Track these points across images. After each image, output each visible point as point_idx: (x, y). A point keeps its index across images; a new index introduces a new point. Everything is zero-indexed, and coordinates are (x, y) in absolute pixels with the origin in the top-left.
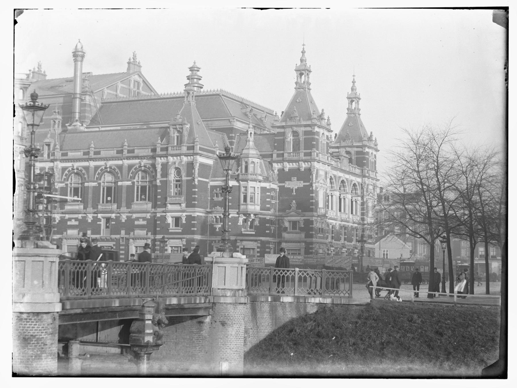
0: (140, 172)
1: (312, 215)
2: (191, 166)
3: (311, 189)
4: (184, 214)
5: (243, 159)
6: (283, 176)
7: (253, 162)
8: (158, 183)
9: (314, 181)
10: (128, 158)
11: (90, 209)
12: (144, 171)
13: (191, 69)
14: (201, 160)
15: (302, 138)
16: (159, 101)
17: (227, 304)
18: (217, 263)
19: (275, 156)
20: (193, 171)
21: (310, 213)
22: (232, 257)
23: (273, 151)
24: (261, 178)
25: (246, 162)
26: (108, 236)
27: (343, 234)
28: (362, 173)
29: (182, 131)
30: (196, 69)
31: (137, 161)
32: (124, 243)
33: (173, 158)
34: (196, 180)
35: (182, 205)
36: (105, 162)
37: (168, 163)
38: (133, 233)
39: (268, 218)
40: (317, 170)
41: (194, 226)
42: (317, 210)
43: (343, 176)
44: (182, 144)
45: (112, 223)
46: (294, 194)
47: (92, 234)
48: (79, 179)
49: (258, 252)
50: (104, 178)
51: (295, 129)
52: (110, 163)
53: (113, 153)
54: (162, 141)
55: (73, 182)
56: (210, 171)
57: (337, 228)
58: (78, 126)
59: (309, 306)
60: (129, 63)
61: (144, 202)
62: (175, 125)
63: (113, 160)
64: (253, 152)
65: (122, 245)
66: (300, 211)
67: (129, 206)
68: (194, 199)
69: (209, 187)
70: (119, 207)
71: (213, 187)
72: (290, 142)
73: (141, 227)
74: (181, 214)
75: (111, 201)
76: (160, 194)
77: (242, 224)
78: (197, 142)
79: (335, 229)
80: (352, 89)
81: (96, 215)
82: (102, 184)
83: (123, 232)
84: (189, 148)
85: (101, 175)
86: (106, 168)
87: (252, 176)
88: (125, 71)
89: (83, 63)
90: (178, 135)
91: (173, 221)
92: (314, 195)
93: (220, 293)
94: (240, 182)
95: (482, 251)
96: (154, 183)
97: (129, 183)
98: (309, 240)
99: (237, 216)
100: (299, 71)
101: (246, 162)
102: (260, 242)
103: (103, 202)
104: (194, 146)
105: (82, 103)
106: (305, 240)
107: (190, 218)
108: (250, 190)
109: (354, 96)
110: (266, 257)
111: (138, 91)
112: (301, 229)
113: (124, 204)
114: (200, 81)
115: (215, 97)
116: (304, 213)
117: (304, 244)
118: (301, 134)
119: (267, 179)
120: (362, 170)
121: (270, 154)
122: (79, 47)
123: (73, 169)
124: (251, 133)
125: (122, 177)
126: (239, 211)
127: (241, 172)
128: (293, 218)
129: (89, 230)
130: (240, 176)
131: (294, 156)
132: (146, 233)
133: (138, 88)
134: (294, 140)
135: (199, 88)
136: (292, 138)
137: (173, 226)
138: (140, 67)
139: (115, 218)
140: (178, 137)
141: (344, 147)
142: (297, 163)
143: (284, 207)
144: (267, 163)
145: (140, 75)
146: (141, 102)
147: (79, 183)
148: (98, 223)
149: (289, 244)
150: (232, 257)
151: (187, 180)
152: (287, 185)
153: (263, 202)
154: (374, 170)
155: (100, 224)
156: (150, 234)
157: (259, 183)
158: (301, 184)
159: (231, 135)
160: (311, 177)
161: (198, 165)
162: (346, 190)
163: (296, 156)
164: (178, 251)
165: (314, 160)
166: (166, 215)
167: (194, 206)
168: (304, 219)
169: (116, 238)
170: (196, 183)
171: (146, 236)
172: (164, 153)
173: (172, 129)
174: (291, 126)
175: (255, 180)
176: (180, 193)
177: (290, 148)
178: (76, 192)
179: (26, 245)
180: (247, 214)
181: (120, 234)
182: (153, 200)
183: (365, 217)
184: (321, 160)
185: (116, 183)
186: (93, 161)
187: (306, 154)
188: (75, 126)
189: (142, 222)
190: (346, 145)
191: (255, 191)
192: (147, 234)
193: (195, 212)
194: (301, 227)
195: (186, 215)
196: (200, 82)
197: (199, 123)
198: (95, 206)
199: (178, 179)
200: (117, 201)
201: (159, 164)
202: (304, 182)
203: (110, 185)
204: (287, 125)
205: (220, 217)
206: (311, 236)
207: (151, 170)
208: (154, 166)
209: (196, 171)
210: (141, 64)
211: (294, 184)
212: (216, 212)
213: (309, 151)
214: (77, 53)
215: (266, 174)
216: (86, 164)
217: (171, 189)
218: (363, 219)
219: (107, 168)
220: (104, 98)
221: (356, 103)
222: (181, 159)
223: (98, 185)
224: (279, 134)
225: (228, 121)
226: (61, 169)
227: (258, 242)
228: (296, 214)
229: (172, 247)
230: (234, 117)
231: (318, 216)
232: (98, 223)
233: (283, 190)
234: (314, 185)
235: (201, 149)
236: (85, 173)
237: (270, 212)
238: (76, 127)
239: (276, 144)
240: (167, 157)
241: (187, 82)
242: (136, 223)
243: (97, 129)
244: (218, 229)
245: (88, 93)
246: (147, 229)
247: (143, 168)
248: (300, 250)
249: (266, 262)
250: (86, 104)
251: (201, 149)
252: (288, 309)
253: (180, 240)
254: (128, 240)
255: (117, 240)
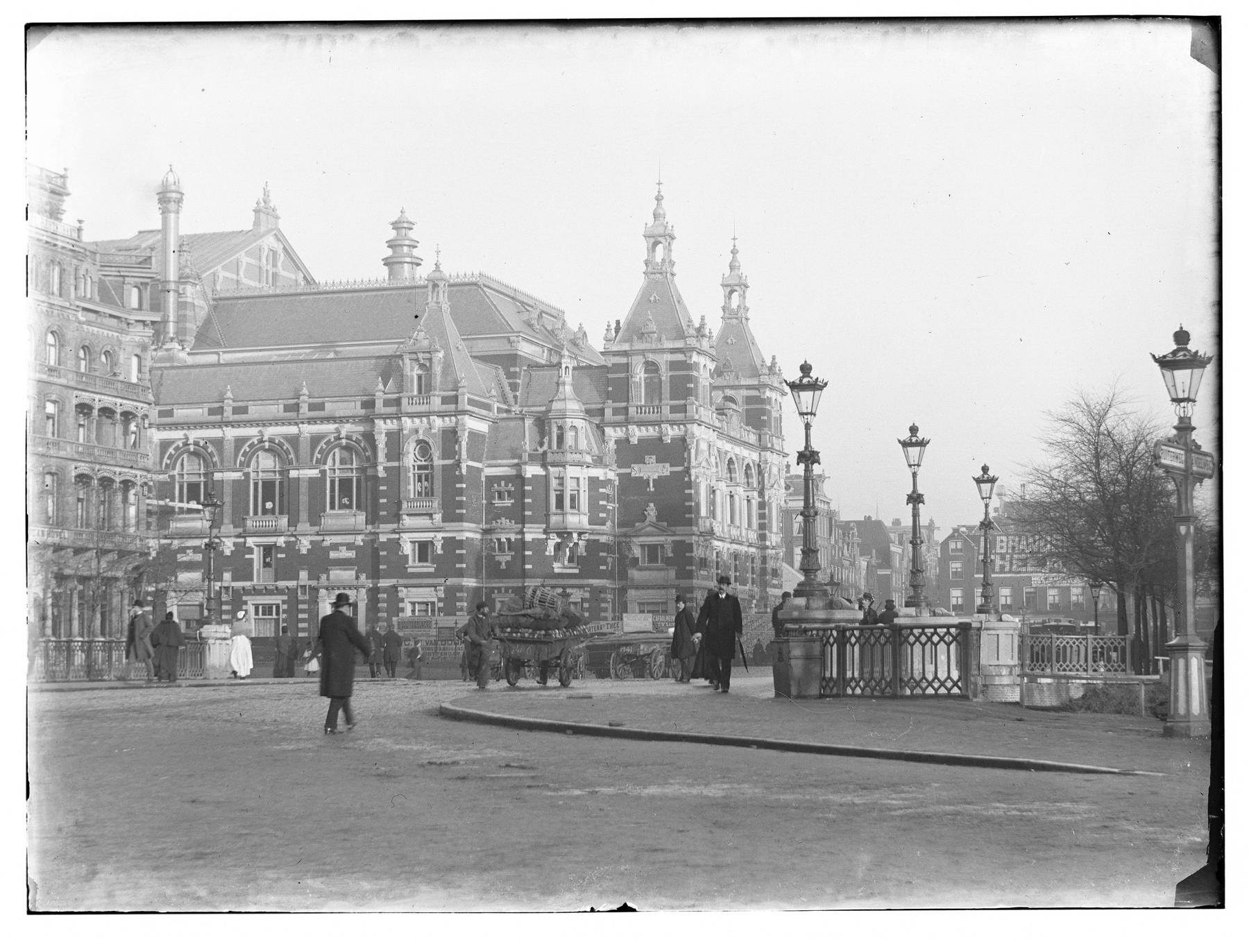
0: (337, 450)
1: (691, 532)
2: (451, 436)
3: (686, 479)
4: (440, 535)
5: (552, 421)
6: (628, 453)
7: (574, 428)
8: (381, 473)
9: (693, 463)
10: (312, 421)
11: (227, 528)
12: (347, 448)
13: (396, 226)
14: (471, 424)
15: (665, 375)
16: (344, 295)
17: (1003, 686)
18: (987, 629)
19: (608, 412)
20: (457, 446)
21: (686, 529)
22: (1001, 620)
23: (604, 403)
24: (588, 459)
25: (560, 428)
26: (271, 584)
27: (733, 569)
28: (760, 441)
29: (431, 365)
30: (406, 225)
31: (330, 427)
32: (307, 597)
33: (413, 422)
34: (464, 466)
35: (434, 516)
36: (259, 428)
37: (400, 430)
38: (325, 575)
39: (603, 539)
40: (697, 441)
41: (461, 559)
42: (697, 520)
43: (729, 449)
44: (432, 393)
45: (279, 556)
46: (652, 489)
47: (234, 579)
48: (200, 464)
49: (605, 610)
50: (257, 462)
51: (651, 357)
52: (270, 431)
53: (276, 410)
54: (385, 387)
55: (185, 471)
56: (484, 445)
57: (725, 558)
58: (176, 351)
59: (1072, 688)
60: (257, 211)
61: (348, 511)
62: (415, 353)
63: (277, 424)
64: (573, 406)
65: (303, 602)
66: (665, 524)
67: (315, 519)
68: (460, 505)
69: (483, 479)
70: (293, 522)
71: (491, 480)
72: (641, 384)
73: (343, 563)
74: (432, 535)
75: (273, 511)
76: (531, 507)
77: (553, 554)
78: (463, 387)
79: (722, 559)
80: (730, 266)
81: (242, 540)
82: (253, 475)
83: (303, 575)
84: (445, 400)
85: (249, 457)
86: (261, 441)
87: (574, 455)
88: (248, 226)
89: (181, 215)
90: (420, 372)
91: (414, 550)
92: (693, 491)
93: (993, 671)
94: (549, 467)
95: (1006, 596)
96: (370, 472)
97: (314, 473)
98: (684, 583)
99: (544, 536)
100: (654, 237)
101: (560, 428)
102: (589, 589)
103: (256, 513)
104: (456, 397)
105: (180, 299)
106: (677, 582)
107: (450, 544)
108: (570, 486)
109: (737, 282)
110: (625, 619)
111: (274, 270)
112: (668, 562)
113: (304, 515)
114: (415, 250)
115: (467, 288)
116: (673, 528)
117: (674, 590)
118: (663, 368)
119: (599, 461)
120: (760, 436)
121: (598, 409)
122: (171, 180)
123: (186, 444)
124: (567, 367)
125: (297, 460)
126: (548, 527)
127: (550, 447)
128: (650, 539)
129: (227, 571)
130: (549, 455)
131: (649, 412)
132: (354, 576)
133: (275, 265)
134: (648, 381)
135: (414, 266)
136: (643, 375)
137: (414, 561)
138: (277, 218)
139: (284, 545)
140: (420, 377)
141: (722, 388)
142: (657, 427)
143: (630, 518)
144: (594, 426)
145: (279, 237)
146: (302, 297)
147: (200, 474)
148: (247, 556)
149: (643, 592)
150: (1001, 620)
151: (443, 466)
152: (637, 471)
153: (594, 507)
154: (780, 436)
155: (252, 560)
156: (363, 577)
157: (585, 470)
158: (666, 470)
159: (512, 369)
160: (686, 456)
161: (467, 434)
162: (736, 478)
163: (653, 412)
164: (426, 611)
165: (693, 421)
166: (399, 539)
167: (460, 519)
168: (673, 541)
169: (287, 588)
170: (464, 471)
171: (355, 583)
172: (392, 410)
173: (407, 361)
174: (643, 352)
175: (579, 464)
176: (429, 493)
177: (641, 396)
178: (193, 491)
179: (921, 613)
180: (564, 534)
181: (297, 578)
182: (369, 508)
183: (767, 532)
184: (702, 419)
185: (284, 472)
186: (233, 426)
187: (674, 409)
188: (167, 350)
189: (345, 554)
190: (725, 383)
191: (578, 485)
192: (357, 578)
193: (462, 531)
194: (668, 558)
195: (443, 538)
196: (415, 252)
197: (460, 347)
198: (239, 521)
199: (424, 463)
200: (288, 507)
201: (381, 433)
202: (671, 466)
203: (270, 476)
204: (633, 348)
205: (509, 540)
206: (690, 575)
207: (362, 445)
208: (370, 437)
209: (463, 447)
210: (278, 212)
211: (652, 470)
212: (499, 531)
213: (682, 402)
214: (169, 195)
215: (596, 451)
216: (215, 433)
217: (409, 484)
218: (763, 537)
219: (264, 442)
220: (218, 288)
221: (740, 296)
222: (429, 423)
223: (243, 478)
224: (617, 368)
225: (506, 341)
226: (159, 444)
227: (586, 589)
228: (656, 530)
229: (413, 604)
230: (519, 332)
231: (701, 534)
232: (247, 556)
233: (629, 485)
234: (693, 472)
235: (471, 402)
236: (215, 453)
237: (604, 527)
238: (171, 352)
239: (610, 389)
240: (399, 419)
241: (389, 252)
242: (333, 555)
243: (212, 358)
244: (504, 564)
245: (191, 280)
246: (356, 568)
247: (344, 442)
248: (666, 603)
249: (626, 629)
250: (186, 302)
251: (471, 402)
252: (1047, 694)
253: (433, 589)
254: (315, 590)
255: (292, 592)
